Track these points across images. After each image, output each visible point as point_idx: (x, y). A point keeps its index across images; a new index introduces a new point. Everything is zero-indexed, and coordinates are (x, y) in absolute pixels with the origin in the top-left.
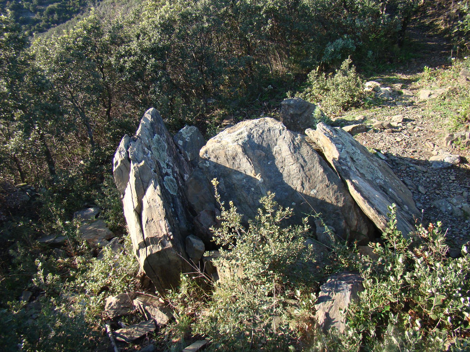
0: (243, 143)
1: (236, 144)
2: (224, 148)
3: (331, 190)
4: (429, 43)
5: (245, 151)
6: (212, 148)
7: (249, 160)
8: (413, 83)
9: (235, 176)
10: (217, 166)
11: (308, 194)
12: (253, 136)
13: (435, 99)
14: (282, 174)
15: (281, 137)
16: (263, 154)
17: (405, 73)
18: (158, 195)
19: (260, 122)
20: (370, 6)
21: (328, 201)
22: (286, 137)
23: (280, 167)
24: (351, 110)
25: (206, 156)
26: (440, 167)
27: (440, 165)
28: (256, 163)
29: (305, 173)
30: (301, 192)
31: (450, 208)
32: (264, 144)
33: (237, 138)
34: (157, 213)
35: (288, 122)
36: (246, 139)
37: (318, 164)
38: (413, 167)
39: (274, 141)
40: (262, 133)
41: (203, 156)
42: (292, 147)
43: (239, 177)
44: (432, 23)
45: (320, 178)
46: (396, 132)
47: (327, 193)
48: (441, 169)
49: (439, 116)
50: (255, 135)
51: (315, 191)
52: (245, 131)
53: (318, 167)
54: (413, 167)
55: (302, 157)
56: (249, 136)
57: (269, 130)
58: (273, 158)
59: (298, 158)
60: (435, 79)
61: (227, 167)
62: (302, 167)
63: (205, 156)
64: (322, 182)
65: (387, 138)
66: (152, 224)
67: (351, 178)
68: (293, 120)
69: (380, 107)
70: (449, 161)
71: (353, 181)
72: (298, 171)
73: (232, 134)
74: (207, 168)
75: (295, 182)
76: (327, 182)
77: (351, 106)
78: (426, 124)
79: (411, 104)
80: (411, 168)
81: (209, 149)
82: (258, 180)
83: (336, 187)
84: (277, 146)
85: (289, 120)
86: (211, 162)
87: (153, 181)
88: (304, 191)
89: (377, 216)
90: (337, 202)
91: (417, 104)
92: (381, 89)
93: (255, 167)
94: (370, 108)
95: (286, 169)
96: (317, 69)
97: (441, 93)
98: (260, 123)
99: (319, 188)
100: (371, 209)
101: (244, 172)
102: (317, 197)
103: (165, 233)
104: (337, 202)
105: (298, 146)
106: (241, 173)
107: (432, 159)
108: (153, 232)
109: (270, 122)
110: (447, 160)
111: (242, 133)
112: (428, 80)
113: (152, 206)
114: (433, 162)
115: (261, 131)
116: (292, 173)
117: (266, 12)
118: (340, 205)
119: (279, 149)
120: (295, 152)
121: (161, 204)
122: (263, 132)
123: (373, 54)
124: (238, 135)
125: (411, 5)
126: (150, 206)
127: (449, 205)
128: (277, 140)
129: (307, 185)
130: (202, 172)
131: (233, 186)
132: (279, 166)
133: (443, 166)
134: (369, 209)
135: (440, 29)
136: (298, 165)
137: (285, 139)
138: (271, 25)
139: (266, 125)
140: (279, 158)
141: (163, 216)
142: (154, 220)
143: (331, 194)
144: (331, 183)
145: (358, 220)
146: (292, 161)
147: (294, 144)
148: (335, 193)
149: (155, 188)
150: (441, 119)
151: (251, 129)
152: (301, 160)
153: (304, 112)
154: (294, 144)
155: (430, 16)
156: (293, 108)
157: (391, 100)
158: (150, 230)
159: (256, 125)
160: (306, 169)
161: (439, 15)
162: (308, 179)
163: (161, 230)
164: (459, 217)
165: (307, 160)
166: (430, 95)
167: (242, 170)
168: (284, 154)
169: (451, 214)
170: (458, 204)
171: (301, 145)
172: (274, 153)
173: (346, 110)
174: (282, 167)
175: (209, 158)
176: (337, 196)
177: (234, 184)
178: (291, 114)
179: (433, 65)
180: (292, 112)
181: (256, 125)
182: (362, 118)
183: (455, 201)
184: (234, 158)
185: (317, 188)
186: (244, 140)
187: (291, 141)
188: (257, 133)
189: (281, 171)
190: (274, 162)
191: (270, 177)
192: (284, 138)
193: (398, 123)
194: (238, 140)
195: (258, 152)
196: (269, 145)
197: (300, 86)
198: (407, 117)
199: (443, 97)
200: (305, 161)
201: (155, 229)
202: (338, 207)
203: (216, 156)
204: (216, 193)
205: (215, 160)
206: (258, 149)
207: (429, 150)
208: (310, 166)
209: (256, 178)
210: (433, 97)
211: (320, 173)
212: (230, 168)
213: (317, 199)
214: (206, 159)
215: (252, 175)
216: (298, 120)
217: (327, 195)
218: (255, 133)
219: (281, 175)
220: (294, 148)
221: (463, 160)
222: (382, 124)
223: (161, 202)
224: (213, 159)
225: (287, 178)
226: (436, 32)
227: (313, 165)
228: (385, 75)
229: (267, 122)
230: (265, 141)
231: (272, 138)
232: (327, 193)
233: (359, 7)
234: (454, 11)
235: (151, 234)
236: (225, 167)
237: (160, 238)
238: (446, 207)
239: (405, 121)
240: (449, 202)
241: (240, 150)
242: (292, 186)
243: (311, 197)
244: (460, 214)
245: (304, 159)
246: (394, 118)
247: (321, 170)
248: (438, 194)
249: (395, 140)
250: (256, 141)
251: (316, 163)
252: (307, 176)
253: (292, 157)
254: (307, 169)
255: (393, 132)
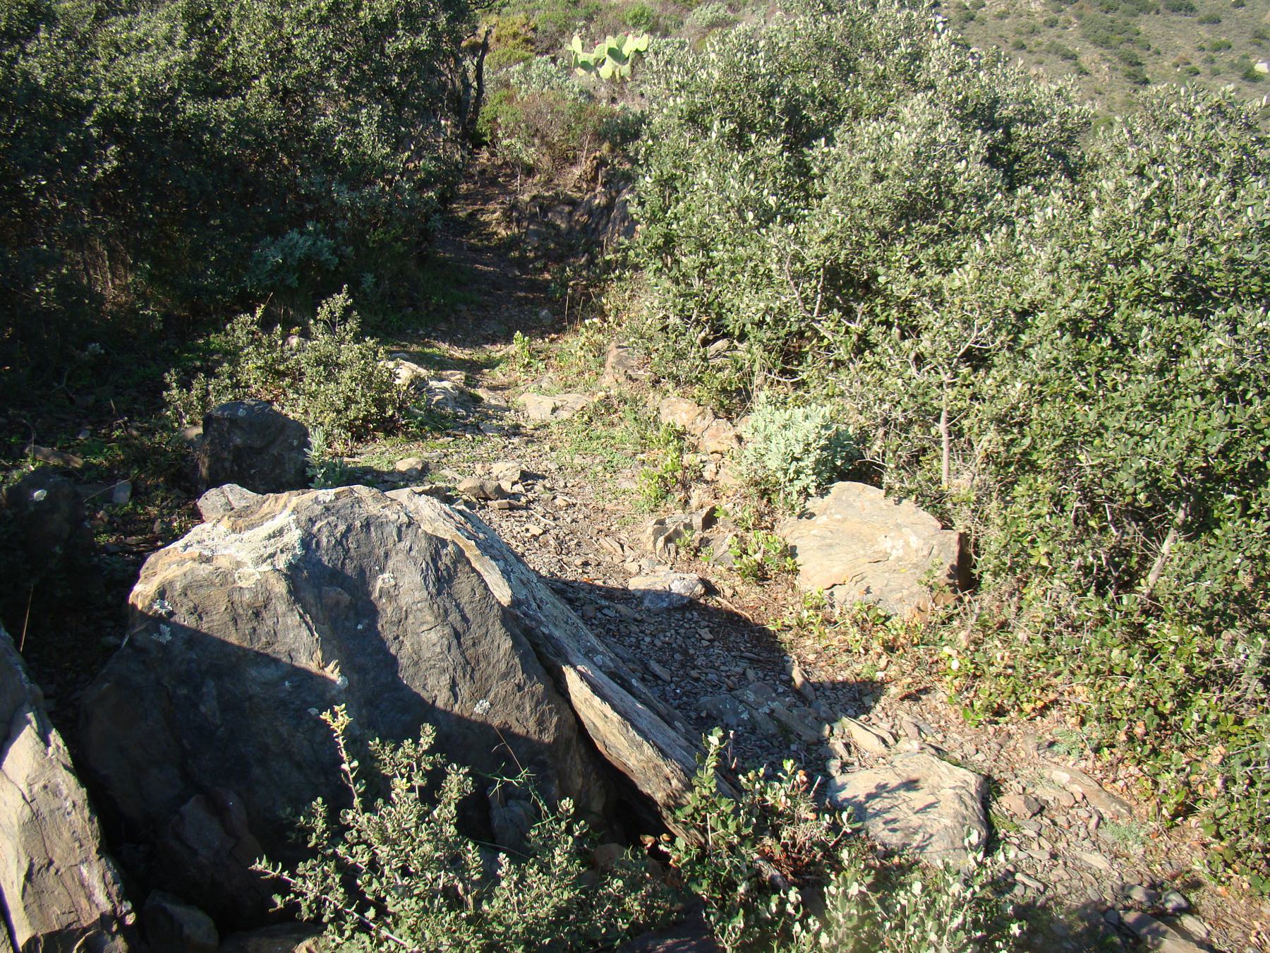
0: (290, 566)
1: (266, 567)
2: (225, 578)
3: (527, 700)
4: (481, 267)
5: (295, 593)
6: (185, 582)
7: (308, 618)
8: (486, 371)
9: (254, 673)
10: (195, 639)
11: (466, 715)
12: (318, 543)
13: (570, 421)
14: (394, 658)
15: (401, 545)
16: (346, 598)
17: (455, 342)
18: (66, 767)
19: (337, 499)
20: (377, 155)
21: (518, 729)
22: (416, 548)
23: (391, 637)
24: (374, 439)
25: (162, 607)
26: (665, 605)
27: (663, 601)
28: (326, 628)
29: (463, 653)
30: (449, 709)
31: (745, 716)
32: (350, 569)
33: (270, 550)
34: (66, 835)
35: (225, 469)
36: (298, 552)
37: (498, 624)
38: (608, 607)
39: (378, 559)
40: (345, 535)
41: (150, 607)
42: (432, 577)
43: (269, 673)
44: (472, 215)
45: (503, 666)
46: (519, 508)
47: (518, 707)
48: (667, 609)
49: (600, 468)
50: (325, 540)
51: (487, 704)
52: (293, 526)
53: (498, 634)
54: (608, 607)
55: (457, 606)
56: (305, 543)
57: (367, 525)
58: (372, 612)
59: (446, 611)
60: (541, 365)
61: (232, 644)
62: (457, 635)
63: (156, 607)
64: (504, 676)
65: (504, 524)
66: (49, 879)
67: (573, 659)
68: (239, 466)
69: (448, 435)
70: (682, 591)
71: (579, 667)
72: (445, 647)
73: (247, 535)
74: (165, 648)
75: (431, 681)
76: (520, 676)
77: (375, 429)
78: (576, 489)
79: (516, 430)
80: (606, 611)
81: (171, 583)
82: (333, 682)
83: (540, 687)
84: (386, 575)
85: (227, 464)
86: (178, 629)
87: (30, 715)
88: (456, 707)
89: (661, 762)
90: (541, 732)
91: (530, 432)
92: (431, 383)
93: (324, 643)
94: (424, 438)
95: (407, 644)
96: (259, 313)
97: (579, 407)
98: (339, 503)
99: (496, 695)
100: (646, 745)
101: (285, 659)
102: (489, 721)
103: (107, 907)
104: (541, 732)
105: (449, 574)
106: (277, 661)
107: (635, 584)
108: (56, 910)
109: (370, 501)
110: (677, 587)
111: (280, 532)
112: (524, 366)
113: (44, 811)
114: (646, 592)
115: (342, 528)
116: (426, 654)
117: (102, 122)
118: (547, 738)
119: (393, 582)
120: (439, 593)
121: (80, 802)
122: (349, 529)
123: (377, 285)
124: (270, 537)
125: (456, 167)
126: (36, 815)
127: (741, 708)
128: (387, 555)
129: (465, 689)
130: (144, 662)
131: (247, 704)
132: (388, 633)
133: (671, 603)
134: (640, 746)
135: (496, 233)
136: (447, 630)
137: (413, 553)
138: (115, 163)
139: (356, 510)
140: (389, 610)
141: (93, 846)
142: (57, 864)
143: (528, 709)
144: (531, 679)
145: (585, 776)
146: (430, 619)
147: (437, 569)
148: (536, 707)
149: (44, 738)
150: (608, 476)
151: (312, 521)
152: (454, 617)
153: (272, 442)
154: (437, 569)
155: (466, 197)
156: (242, 428)
157: (463, 418)
158: (40, 906)
159: (327, 509)
160: (467, 641)
161: (487, 200)
162: (469, 669)
163: (89, 897)
164: (773, 736)
165: (469, 616)
166: (554, 410)
167: (279, 650)
168: (405, 600)
169: (753, 731)
170: (761, 705)
171: (455, 571)
172: (376, 594)
173: (359, 438)
174: (397, 638)
175: (171, 614)
176: (543, 714)
177: (250, 698)
178: (236, 447)
179: (534, 329)
180: (239, 441)
181: (327, 509)
182: (419, 467)
183: (751, 696)
184: (257, 614)
185: (492, 695)
186: (294, 556)
187: (428, 559)
188: (331, 534)
189: (393, 651)
190: (374, 622)
191: (361, 670)
192: (411, 549)
193: (514, 483)
194: (272, 556)
195: (334, 594)
196: (362, 571)
197: (181, 352)
198: (532, 468)
199: (586, 418)
200: (465, 619)
201: (65, 901)
202: (543, 743)
203: (196, 608)
204: (344, 754)
205: (188, 621)
206: (331, 584)
207: (617, 561)
208: (479, 632)
209: (324, 678)
210: (564, 415)
211: (502, 652)
212: (239, 648)
213: (490, 726)
214: (159, 619)
215: (313, 667)
216: (251, 467)
217: (516, 713)
218: (325, 532)
219: (393, 662)
220: (438, 579)
221: (710, 590)
222: (482, 487)
223: (80, 794)
224: (184, 619)
225: (411, 671)
226: (488, 240)
227: (484, 630)
228: (411, 343)
229: (359, 501)
230: (352, 559)
231: (373, 548)
232: (518, 707)
233: (345, 151)
234: (526, 197)
235: (46, 919)
236: (224, 643)
237: (85, 930)
238: (737, 714)
239: (525, 476)
240: (741, 702)
241: (280, 587)
242: (424, 694)
243: (475, 722)
244: (772, 728)
245: (461, 611)
246: (498, 468)
247: (508, 644)
248: (697, 680)
249: (527, 530)
250: (325, 559)
251: (493, 624)
252: (468, 663)
253: (431, 607)
254: (470, 642)
255: (512, 508)
